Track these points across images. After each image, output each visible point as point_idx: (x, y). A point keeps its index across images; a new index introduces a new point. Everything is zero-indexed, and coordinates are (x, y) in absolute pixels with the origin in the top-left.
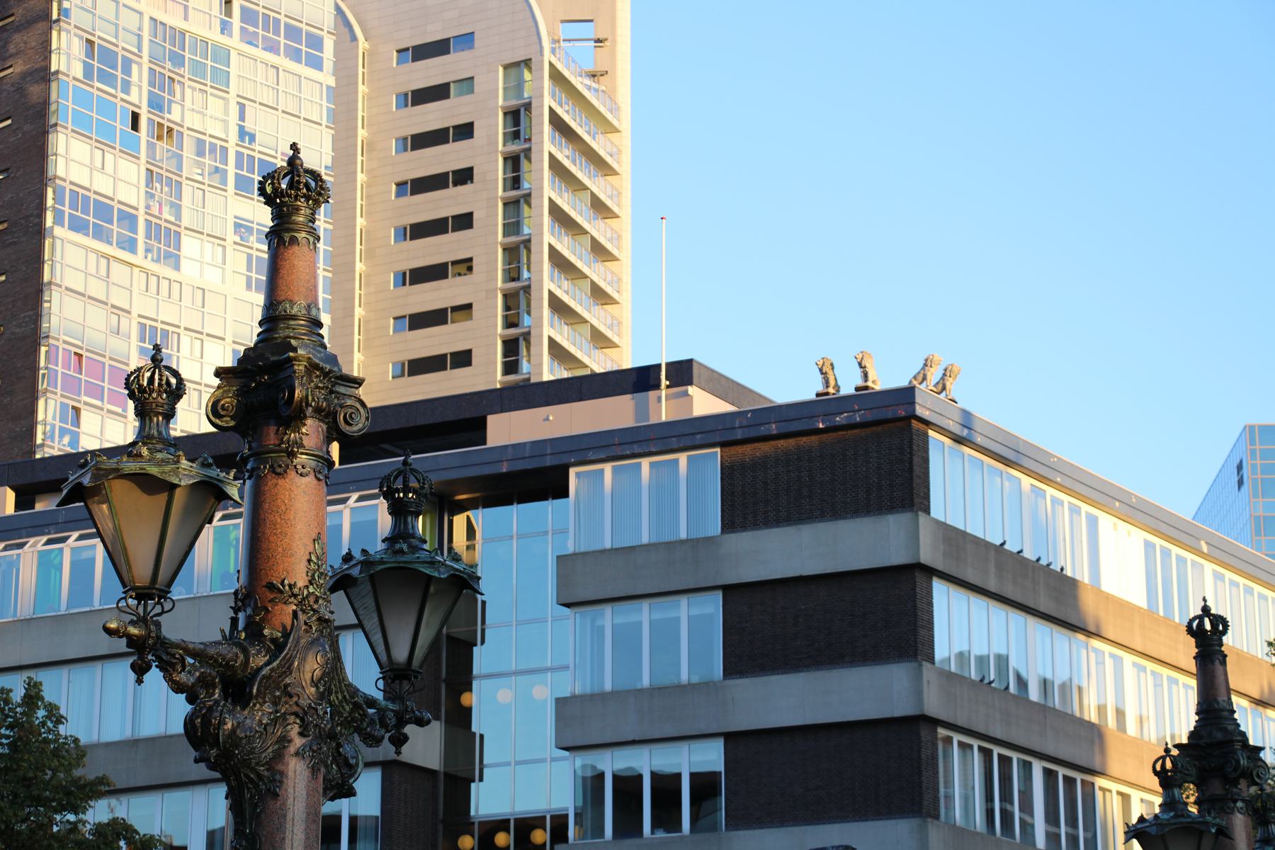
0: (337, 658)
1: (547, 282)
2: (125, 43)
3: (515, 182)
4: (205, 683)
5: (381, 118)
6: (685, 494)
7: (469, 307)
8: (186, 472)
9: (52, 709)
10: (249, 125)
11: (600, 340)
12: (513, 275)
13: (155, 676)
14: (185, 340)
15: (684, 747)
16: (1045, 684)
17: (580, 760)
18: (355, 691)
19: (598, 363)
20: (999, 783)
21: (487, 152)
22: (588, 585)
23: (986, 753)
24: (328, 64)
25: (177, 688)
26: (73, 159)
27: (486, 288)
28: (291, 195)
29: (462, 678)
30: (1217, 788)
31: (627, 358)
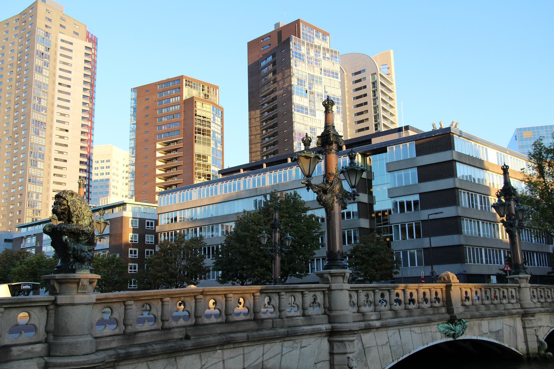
0: (342, 185)
1: (382, 113)
2: (304, 78)
3: (375, 95)
4: (320, 191)
5: (350, 86)
6: (408, 151)
7: (368, 119)
8: (312, 155)
9: (299, 195)
10: (326, 90)
11: (392, 123)
12: (375, 112)
13: (310, 190)
14: (318, 129)
15: (412, 196)
16: (479, 179)
17: (393, 199)
18: (345, 191)
19: (392, 127)
20: (471, 199)
21: (369, 91)
22: (392, 168)
23: (468, 193)
24: (339, 78)
25: (315, 192)
26: (297, 100)
27: (371, 115)
28: (328, 104)
29: (370, 186)
30: (508, 197)
31: (398, 126)
